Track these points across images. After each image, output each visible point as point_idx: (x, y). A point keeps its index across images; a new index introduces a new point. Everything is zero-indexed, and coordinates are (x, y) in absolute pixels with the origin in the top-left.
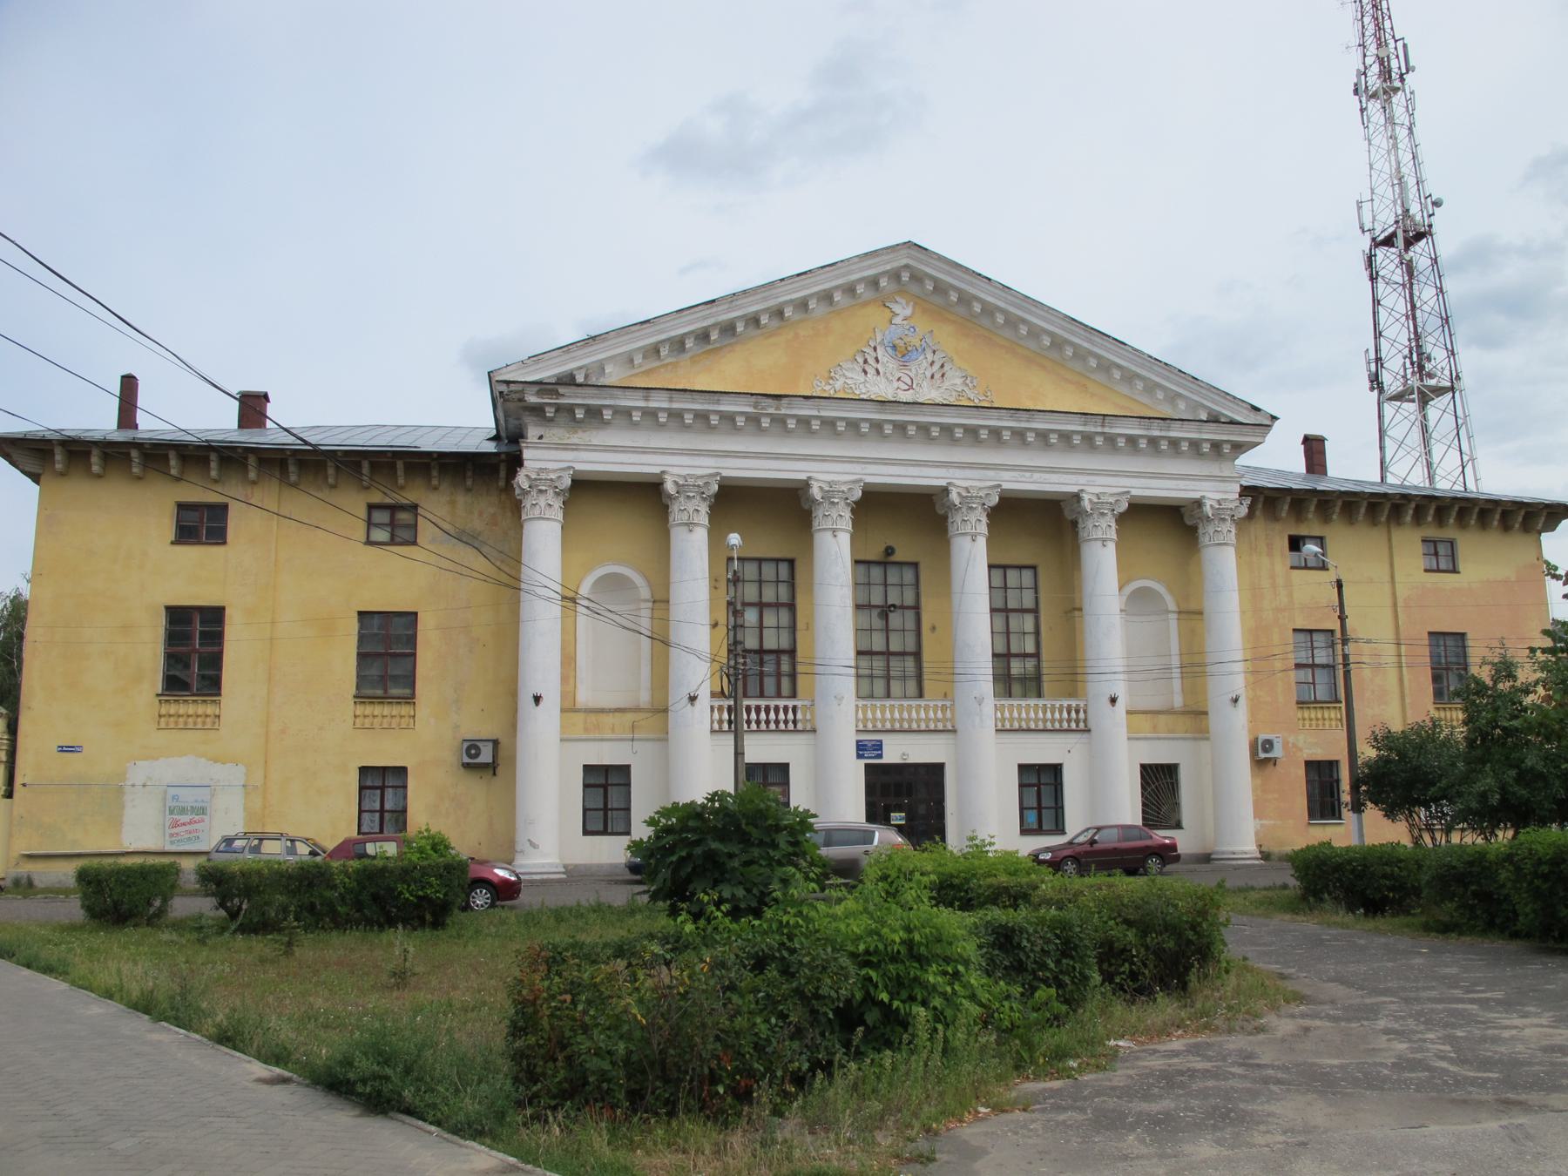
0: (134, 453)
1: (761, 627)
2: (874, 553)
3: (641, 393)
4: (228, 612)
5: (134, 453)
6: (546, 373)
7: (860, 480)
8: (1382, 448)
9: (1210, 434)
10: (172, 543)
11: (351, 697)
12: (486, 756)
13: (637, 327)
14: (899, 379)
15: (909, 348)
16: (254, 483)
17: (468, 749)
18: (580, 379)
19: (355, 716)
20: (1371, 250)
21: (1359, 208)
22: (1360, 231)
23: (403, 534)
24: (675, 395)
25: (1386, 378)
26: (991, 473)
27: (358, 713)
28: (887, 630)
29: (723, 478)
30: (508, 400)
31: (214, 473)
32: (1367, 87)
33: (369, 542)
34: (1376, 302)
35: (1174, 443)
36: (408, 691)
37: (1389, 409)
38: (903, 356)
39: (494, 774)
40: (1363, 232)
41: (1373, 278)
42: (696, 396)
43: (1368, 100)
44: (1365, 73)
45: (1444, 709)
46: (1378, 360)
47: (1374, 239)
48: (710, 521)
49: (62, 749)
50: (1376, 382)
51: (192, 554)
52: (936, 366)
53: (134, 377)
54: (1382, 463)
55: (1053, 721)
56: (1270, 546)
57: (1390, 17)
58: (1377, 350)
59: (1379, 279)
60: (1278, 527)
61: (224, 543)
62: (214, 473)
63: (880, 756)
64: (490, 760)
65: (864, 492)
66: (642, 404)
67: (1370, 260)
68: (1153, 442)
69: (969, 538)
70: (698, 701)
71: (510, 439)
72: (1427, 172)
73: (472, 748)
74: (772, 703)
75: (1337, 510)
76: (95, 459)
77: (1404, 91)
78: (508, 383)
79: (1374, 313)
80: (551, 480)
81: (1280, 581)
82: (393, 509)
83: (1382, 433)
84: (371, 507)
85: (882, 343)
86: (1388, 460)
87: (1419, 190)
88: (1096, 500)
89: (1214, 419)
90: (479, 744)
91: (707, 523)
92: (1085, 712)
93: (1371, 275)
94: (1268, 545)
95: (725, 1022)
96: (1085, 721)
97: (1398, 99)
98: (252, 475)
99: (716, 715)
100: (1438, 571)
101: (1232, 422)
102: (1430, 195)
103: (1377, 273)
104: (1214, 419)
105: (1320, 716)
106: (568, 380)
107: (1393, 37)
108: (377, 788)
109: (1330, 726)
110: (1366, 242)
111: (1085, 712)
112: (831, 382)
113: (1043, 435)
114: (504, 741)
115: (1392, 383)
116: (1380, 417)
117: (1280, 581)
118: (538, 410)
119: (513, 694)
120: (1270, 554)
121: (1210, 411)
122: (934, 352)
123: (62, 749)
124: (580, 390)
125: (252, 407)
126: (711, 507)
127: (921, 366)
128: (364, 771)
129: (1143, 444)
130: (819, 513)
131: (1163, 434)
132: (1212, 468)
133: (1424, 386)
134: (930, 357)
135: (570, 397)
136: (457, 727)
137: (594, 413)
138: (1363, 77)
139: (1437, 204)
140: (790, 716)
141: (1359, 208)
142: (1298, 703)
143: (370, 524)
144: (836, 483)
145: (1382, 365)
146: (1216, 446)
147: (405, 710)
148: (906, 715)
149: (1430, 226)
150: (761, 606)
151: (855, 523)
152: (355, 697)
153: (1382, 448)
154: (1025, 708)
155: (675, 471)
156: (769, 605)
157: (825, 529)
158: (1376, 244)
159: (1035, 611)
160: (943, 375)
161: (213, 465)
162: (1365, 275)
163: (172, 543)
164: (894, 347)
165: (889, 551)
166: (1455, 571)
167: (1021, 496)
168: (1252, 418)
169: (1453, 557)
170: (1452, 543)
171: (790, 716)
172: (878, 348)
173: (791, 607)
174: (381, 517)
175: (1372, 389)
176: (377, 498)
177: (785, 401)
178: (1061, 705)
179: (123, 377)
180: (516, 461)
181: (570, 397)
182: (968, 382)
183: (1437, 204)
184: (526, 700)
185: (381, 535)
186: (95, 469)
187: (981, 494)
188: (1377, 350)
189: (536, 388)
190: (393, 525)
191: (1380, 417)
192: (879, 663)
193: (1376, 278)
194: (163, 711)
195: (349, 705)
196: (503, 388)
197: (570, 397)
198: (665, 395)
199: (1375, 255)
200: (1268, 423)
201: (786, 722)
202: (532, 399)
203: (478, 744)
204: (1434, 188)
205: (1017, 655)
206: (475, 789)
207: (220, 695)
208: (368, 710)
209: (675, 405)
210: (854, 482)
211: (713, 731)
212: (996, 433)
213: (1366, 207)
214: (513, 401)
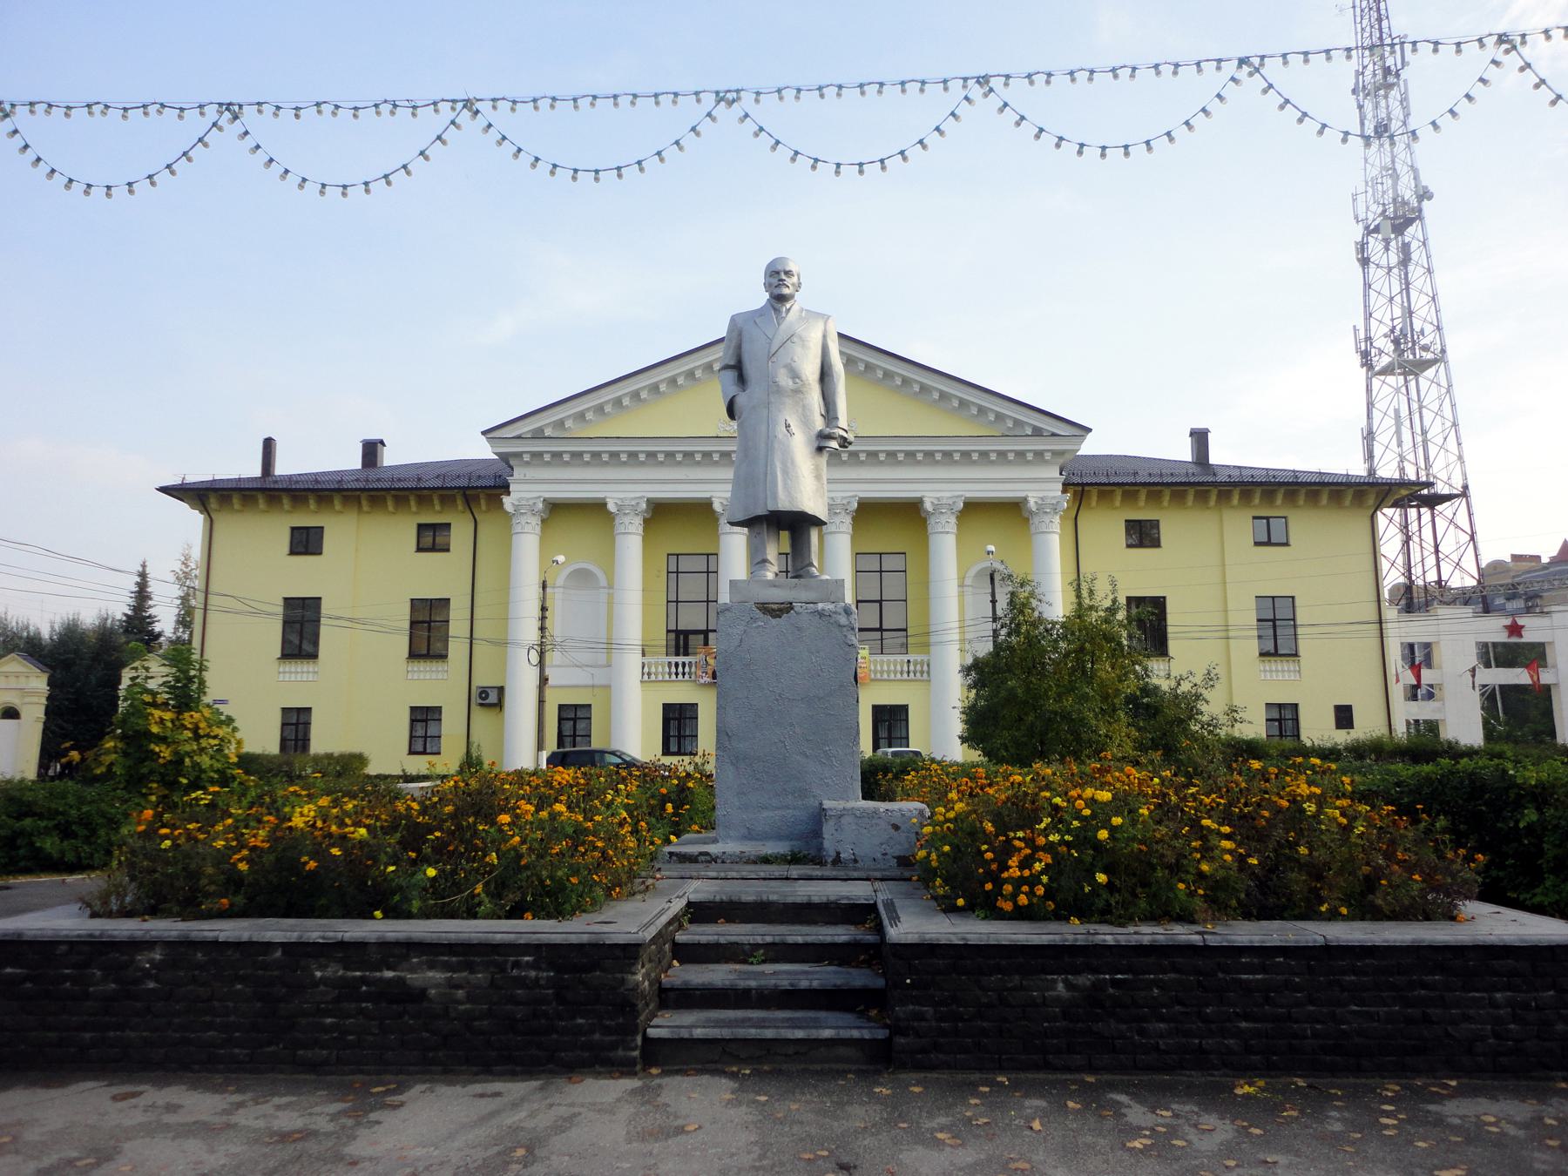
7: (539, 497)
12: (493, 698)
17: (481, 693)
27: (410, 669)
29: (860, 498)
32: (1364, 86)
34: (1367, 286)
37: (1376, 382)
40: (1358, 222)
43: (1365, 98)
44: (1363, 73)
46: (1368, 339)
47: (1367, 228)
48: (1061, 529)
50: (1366, 359)
55: (902, 673)
57: (1387, 17)
58: (1367, 329)
64: (496, 701)
65: (859, 503)
67: (1362, 247)
77: (1399, 86)
79: (1365, 296)
90: (489, 691)
91: (955, 531)
92: (928, 665)
96: (928, 673)
97: (1394, 93)
105: (1280, 668)
107: (1390, 36)
110: (1358, 232)
111: (928, 665)
116: (1369, 390)
126: (854, 519)
128: (413, 709)
130: (932, 521)
138: (1361, 77)
142: (1261, 655)
145: (1371, 344)
148: (885, 668)
151: (959, 526)
155: (718, 494)
157: (948, 533)
167: (585, 501)
175: (1362, 366)
188: (1367, 329)
194: (281, 670)
199: (1367, 243)
201: (677, 674)
210: (853, 497)
213: (1361, 198)
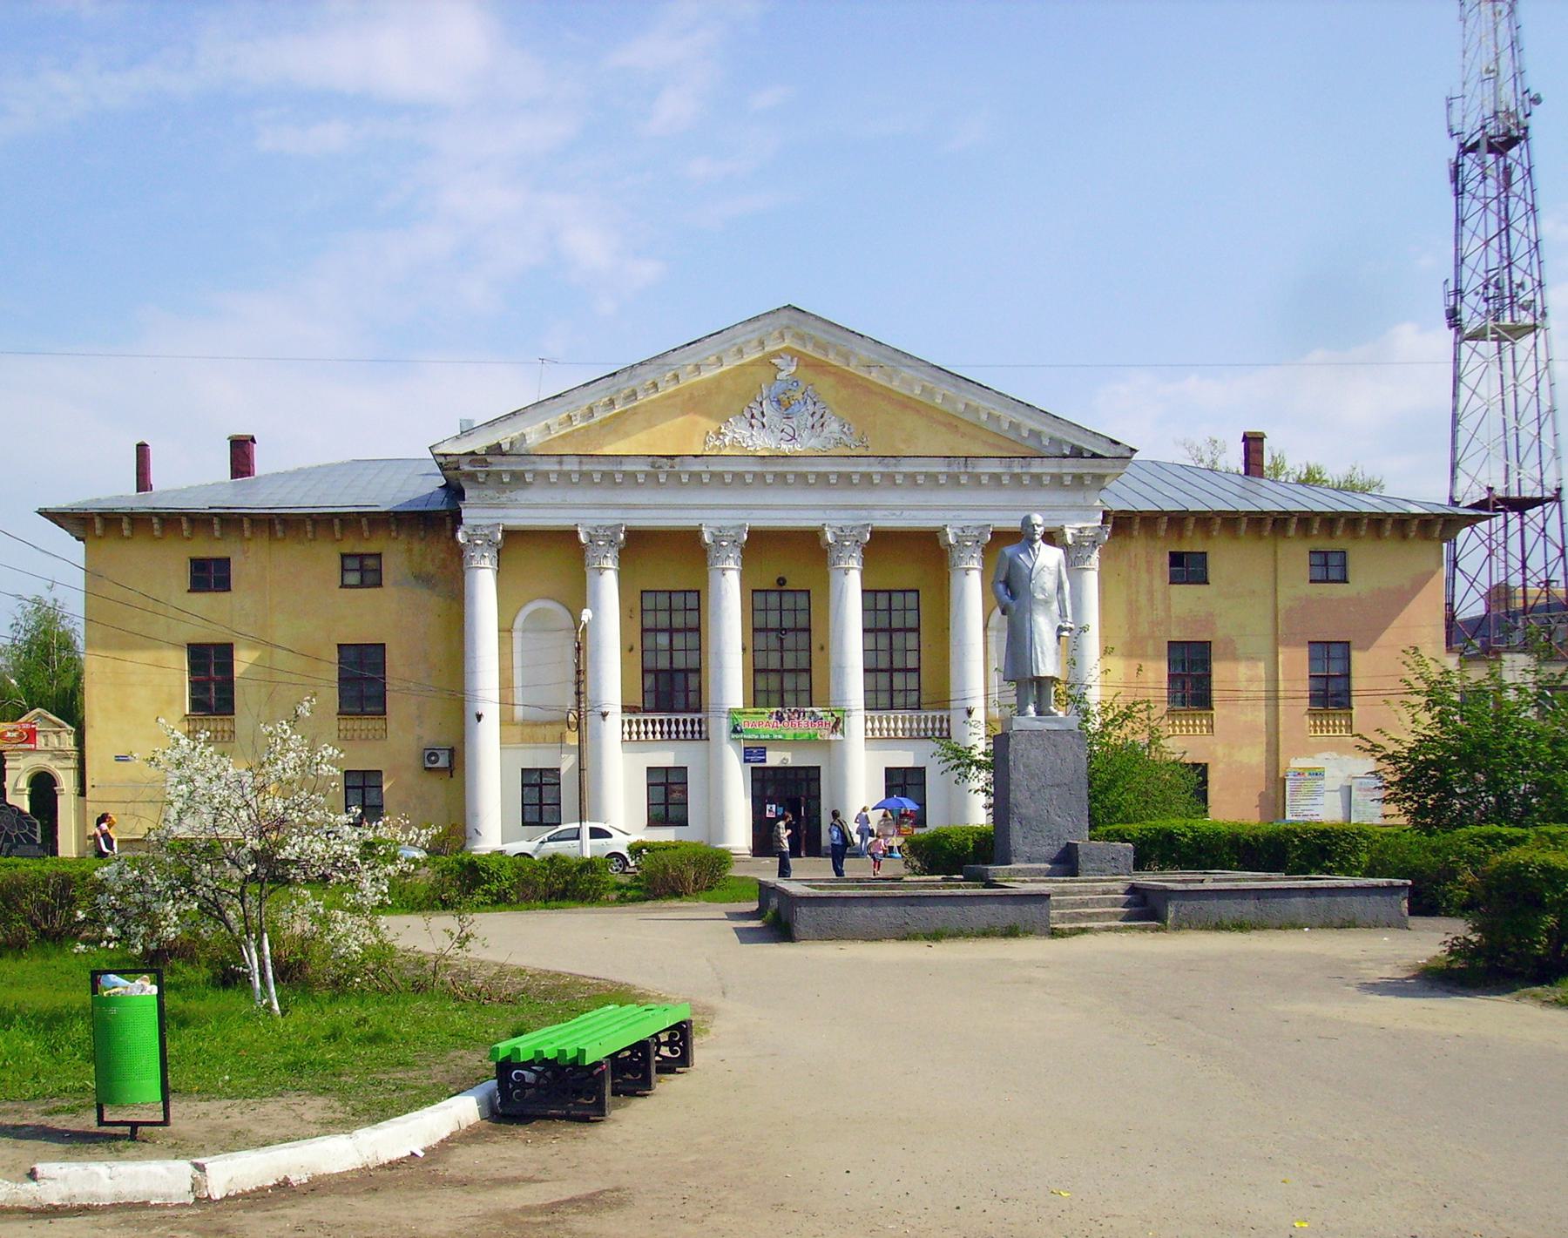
0: (155, 520)
1: (671, 649)
2: (769, 582)
3: (555, 459)
4: (226, 595)
5: (155, 520)
6: (478, 444)
8: (1455, 395)
9: (1070, 467)
10: (189, 591)
11: (335, 714)
13: (551, 401)
14: (782, 431)
15: (792, 402)
16: (249, 539)
17: (430, 755)
18: (506, 447)
19: (339, 730)
20: (1458, 158)
21: (1449, 106)
22: (1448, 135)
23: (370, 578)
24: (584, 459)
25: (1465, 314)
26: (864, 513)
28: (782, 649)
30: (446, 470)
31: (217, 534)
33: (343, 586)
35: (1037, 478)
36: (381, 709)
38: (787, 409)
39: (452, 776)
40: (1452, 136)
41: (1459, 193)
42: (602, 459)
45: (1328, 714)
46: (1458, 292)
47: (1462, 145)
49: (118, 759)
50: (1453, 317)
51: (203, 600)
52: (817, 416)
53: (146, 445)
54: (1455, 415)
56: (1149, 563)
58: (1458, 280)
59: (1466, 195)
60: (1160, 544)
61: (229, 589)
62: (217, 534)
63: (764, 761)
66: (557, 468)
67: (1456, 171)
68: (1016, 478)
69: (843, 571)
70: (608, 717)
71: (454, 491)
72: (1529, 60)
73: (432, 754)
74: (681, 717)
75: (1217, 527)
76: (125, 525)
78: (445, 455)
80: (485, 535)
81: (1158, 596)
82: (361, 557)
83: (1457, 379)
84: (344, 556)
85: (769, 396)
86: (1460, 411)
87: (1515, 85)
88: (961, 534)
89: (1077, 453)
92: (948, 721)
93: (1456, 189)
94: (1148, 562)
95: (256, 844)
98: (247, 534)
99: (626, 728)
100: (1327, 581)
101: (1094, 456)
102: (1528, 91)
103: (1464, 186)
104: (1077, 453)
106: (496, 450)
108: (358, 787)
109: (1181, 731)
112: (721, 437)
113: (911, 478)
114: (457, 747)
115: (1471, 322)
117: (1158, 596)
118: (472, 477)
119: (462, 711)
120: (1149, 571)
121: (1073, 447)
122: (815, 404)
123: (118, 759)
124: (504, 459)
125: (241, 453)
127: (803, 417)
129: (1006, 479)
131: (1024, 470)
132: (1077, 498)
133: (1498, 326)
134: (811, 408)
135: (498, 465)
136: (420, 738)
137: (518, 478)
139: (1536, 101)
140: (696, 728)
141: (1449, 106)
143: (344, 570)
144: (724, 528)
146: (1078, 478)
147: (378, 724)
149: (1526, 129)
150: (671, 631)
152: (338, 714)
153: (1455, 395)
154: (898, 720)
156: (678, 630)
158: (1465, 149)
159: (917, 630)
160: (822, 425)
161: (216, 527)
162: (1450, 188)
163: (189, 591)
164: (778, 402)
165: (781, 581)
166: (1345, 581)
168: (1118, 451)
169: (1343, 566)
170: (1343, 554)
171: (696, 728)
172: (764, 403)
173: (698, 630)
174: (355, 564)
176: (347, 550)
177: (677, 459)
178: (942, 716)
179: (138, 445)
180: (457, 519)
181: (496, 465)
182: (845, 430)
183: (1536, 101)
184: (471, 718)
185: (353, 578)
186: (126, 533)
187: (854, 533)
188: (1458, 280)
189: (469, 458)
190: (362, 570)
191: (1456, 360)
192: (774, 681)
193: (1462, 193)
195: (334, 721)
196: (442, 460)
197: (498, 465)
198: (576, 459)
200: (1129, 455)
202: (466, 468)
203: (438, 752)
204: (1534, 84)
205: (899, 670)
206: (435, 785)
207: (233, 714)
208: (350, 724)
209: (585, 468)
211: (623, 741)
212: (867, 477)
213: (1457, 103)
214: (450, 469)
